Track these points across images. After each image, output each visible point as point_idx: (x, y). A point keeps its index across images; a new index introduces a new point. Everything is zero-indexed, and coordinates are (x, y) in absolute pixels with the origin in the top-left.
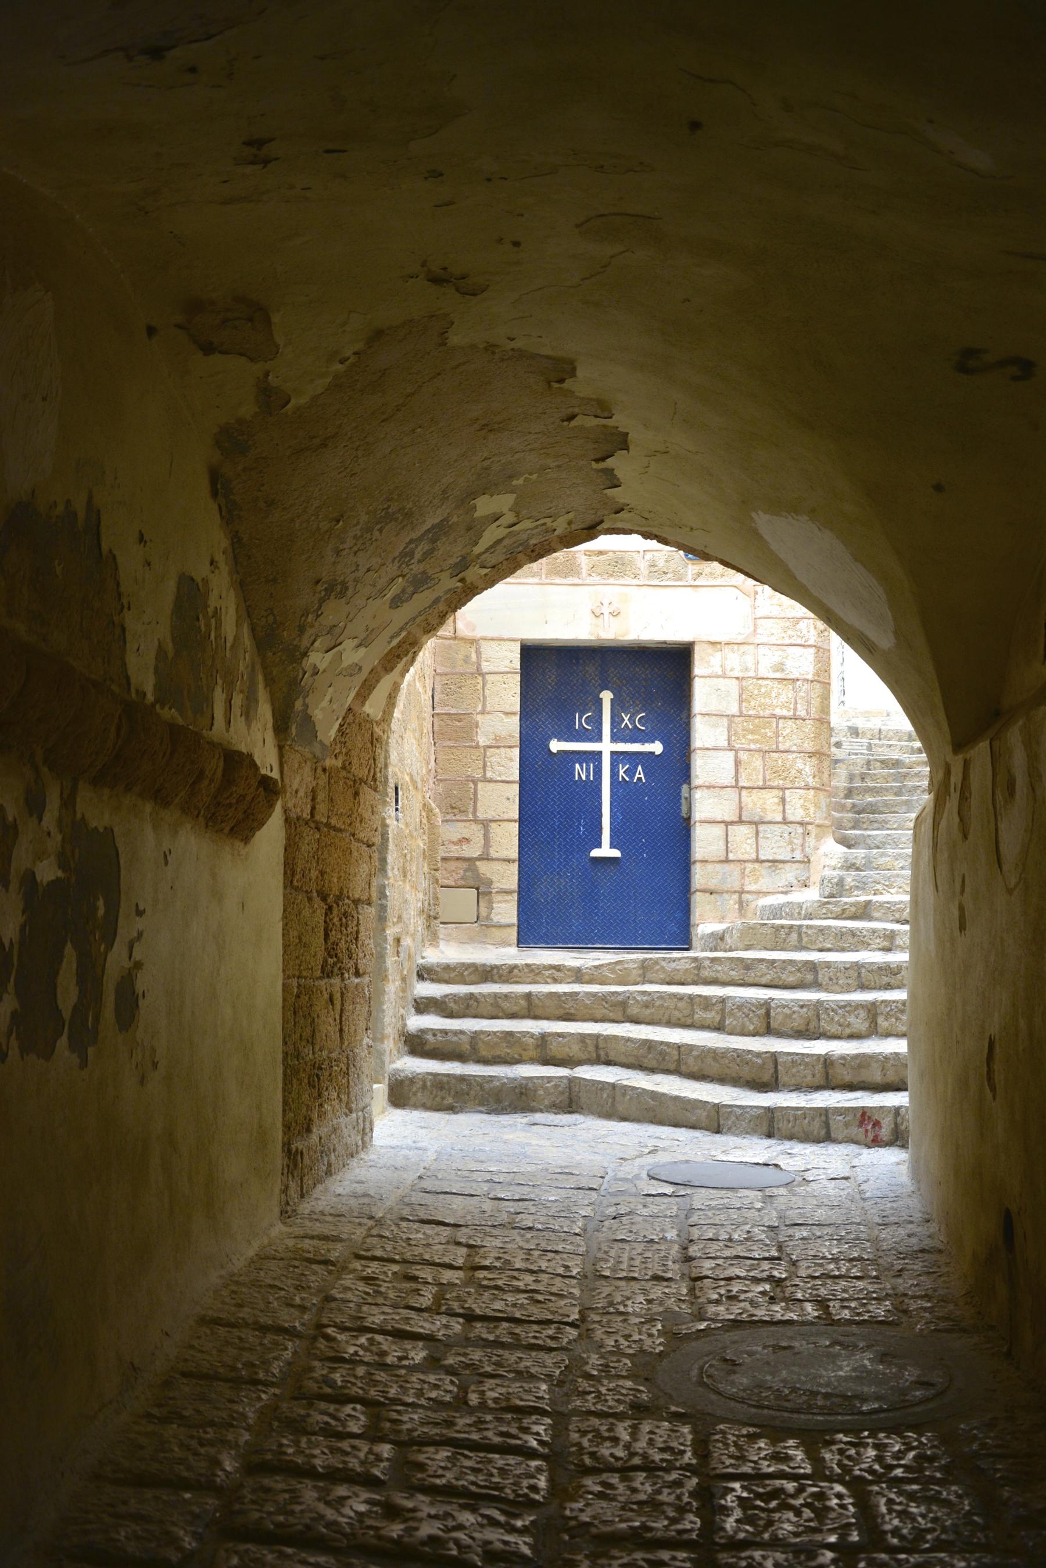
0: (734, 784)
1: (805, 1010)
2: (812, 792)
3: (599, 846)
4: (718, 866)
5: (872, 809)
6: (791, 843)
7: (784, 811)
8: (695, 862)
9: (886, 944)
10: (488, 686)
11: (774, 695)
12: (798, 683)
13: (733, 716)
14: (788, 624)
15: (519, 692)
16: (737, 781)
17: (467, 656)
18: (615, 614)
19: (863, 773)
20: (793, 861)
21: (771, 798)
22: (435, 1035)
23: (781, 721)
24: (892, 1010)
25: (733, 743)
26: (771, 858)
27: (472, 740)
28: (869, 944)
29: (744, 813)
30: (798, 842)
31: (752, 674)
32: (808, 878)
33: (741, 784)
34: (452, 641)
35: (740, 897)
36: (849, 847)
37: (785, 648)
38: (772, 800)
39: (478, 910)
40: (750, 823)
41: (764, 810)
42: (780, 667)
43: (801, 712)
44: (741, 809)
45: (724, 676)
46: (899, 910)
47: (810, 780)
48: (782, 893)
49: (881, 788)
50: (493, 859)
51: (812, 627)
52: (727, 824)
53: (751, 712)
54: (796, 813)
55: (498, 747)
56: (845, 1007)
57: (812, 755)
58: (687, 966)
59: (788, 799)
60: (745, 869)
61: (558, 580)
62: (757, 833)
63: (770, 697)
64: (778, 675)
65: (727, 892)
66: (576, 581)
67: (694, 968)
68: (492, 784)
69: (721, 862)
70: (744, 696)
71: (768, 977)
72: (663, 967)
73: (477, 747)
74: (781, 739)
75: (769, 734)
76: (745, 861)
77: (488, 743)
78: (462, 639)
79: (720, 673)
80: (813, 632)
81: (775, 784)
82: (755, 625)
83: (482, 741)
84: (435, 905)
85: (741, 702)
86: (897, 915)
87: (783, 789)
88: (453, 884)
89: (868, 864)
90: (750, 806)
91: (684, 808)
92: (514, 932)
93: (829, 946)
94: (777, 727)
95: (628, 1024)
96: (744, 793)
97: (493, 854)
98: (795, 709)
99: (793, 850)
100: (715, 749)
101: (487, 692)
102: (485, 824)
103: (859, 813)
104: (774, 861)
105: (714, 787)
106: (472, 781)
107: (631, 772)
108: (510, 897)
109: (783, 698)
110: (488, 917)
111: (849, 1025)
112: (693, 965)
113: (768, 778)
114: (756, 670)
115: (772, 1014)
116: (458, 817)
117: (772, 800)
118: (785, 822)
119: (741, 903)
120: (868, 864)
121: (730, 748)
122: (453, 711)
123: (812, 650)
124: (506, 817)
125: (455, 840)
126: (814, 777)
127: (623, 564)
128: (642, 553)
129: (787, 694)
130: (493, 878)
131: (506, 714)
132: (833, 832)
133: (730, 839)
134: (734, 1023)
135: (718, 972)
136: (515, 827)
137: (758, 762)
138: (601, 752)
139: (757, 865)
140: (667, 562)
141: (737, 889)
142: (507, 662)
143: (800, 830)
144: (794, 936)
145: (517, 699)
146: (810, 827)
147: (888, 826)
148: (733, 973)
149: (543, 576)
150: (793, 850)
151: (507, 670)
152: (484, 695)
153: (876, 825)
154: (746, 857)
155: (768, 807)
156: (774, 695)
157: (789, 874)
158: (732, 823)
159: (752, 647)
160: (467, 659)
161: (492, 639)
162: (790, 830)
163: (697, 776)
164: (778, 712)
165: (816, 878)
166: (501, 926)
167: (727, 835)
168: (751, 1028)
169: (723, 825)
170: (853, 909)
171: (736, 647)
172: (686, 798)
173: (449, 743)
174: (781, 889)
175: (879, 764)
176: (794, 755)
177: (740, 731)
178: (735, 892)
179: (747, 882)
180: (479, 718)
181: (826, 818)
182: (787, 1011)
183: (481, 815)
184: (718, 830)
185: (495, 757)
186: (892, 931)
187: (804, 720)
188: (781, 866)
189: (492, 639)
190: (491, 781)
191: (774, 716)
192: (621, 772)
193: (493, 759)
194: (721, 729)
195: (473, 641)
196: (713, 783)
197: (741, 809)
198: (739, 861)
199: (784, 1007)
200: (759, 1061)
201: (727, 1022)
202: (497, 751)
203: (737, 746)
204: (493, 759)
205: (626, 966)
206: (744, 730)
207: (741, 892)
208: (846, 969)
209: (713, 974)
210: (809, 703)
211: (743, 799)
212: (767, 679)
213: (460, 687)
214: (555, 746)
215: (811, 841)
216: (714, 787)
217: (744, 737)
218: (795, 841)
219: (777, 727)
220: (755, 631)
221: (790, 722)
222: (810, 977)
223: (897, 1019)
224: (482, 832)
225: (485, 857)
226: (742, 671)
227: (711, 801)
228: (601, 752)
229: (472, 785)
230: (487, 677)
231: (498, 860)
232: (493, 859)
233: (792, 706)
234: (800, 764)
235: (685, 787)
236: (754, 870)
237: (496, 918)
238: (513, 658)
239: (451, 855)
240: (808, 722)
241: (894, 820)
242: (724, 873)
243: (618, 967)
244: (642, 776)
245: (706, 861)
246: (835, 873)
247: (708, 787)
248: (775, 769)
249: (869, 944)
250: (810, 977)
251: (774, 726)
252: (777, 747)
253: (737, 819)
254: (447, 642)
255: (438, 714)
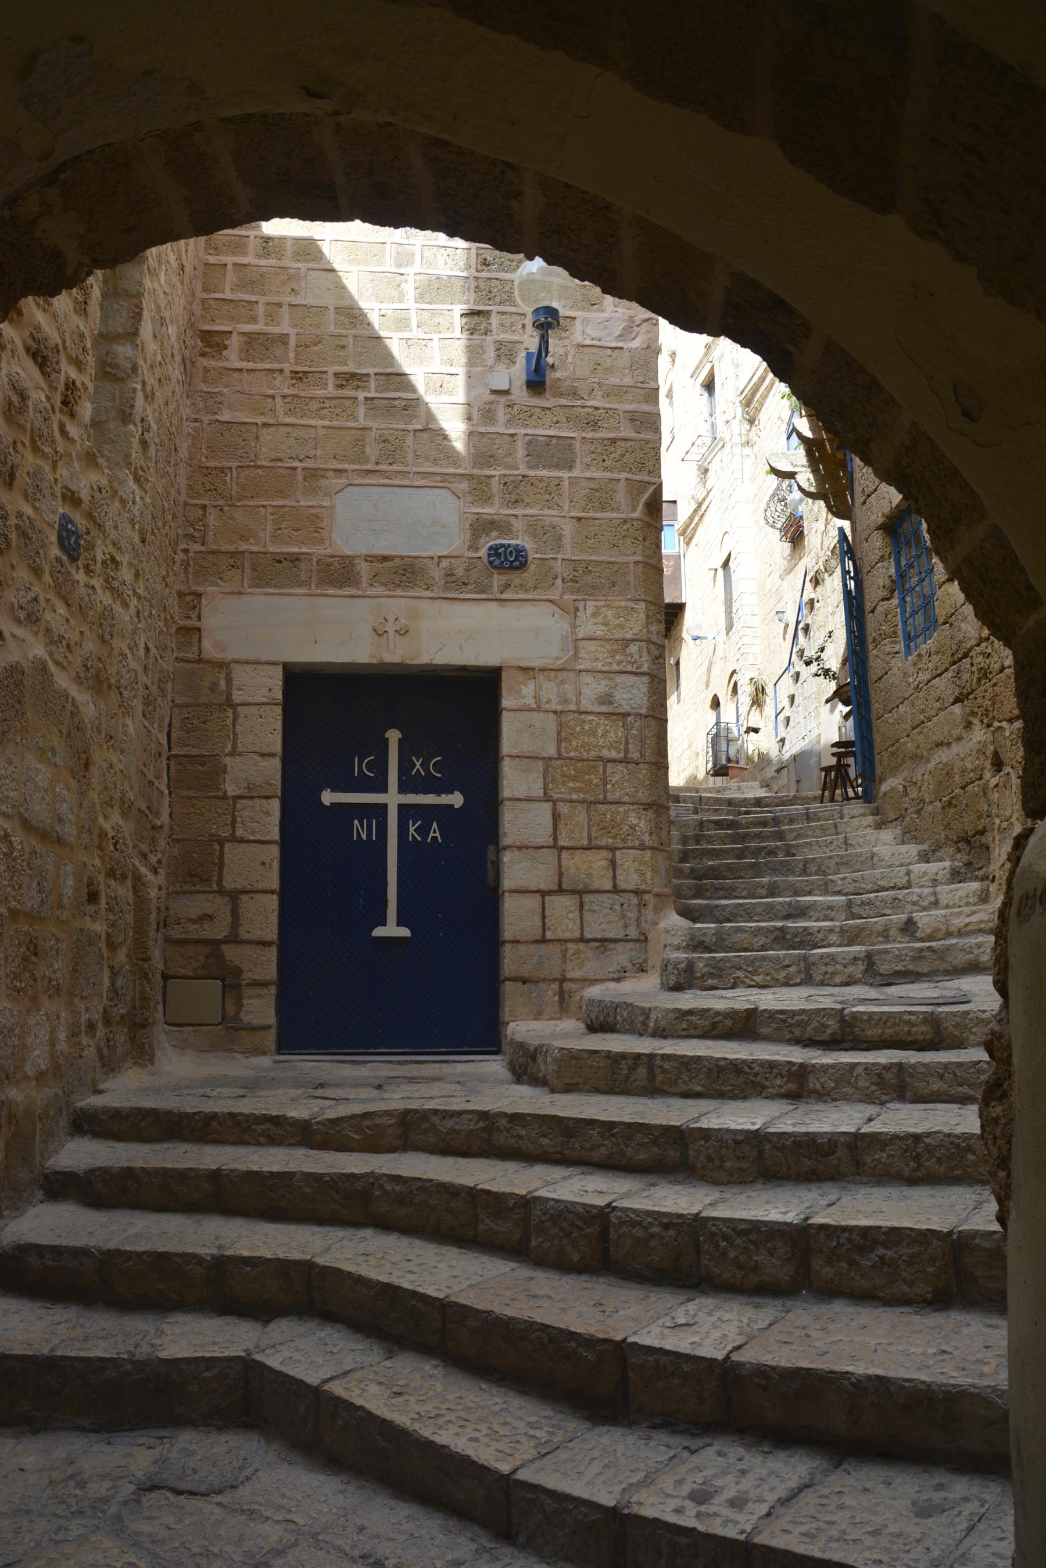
0: (552, 843)
1: (672, 1233)
2: (649, 853)
3: (384, 923)
4: (533, 948)
5: (715, 873)
6: (623, 917)
7: (614, 877)
8: (504, 942)
9: (792, 1086)
10: (240, 721)
11: (600, 733)
12: (630, 719)
13: (550, 759)
14: (615, 647)
15: (280, 728)
16: (555, 839)
17: (214, 684)
18: (403, 632)
19: (697, 835)
20: (626, 940)
21: (598, 861)
22: (41, 1256)
23: (609, 765)
24: (840, 1245)
25: (551, 793)
26: (599, 936)
27: (218, 789)
28: (764, 1088)
29: (565, 880)
30: (632, 915)
31: (572, 707)
32: (645, 961)
33: (561, 843)
34: (196, 665)
35: (561, 987)
36: (694, 920)
37: (613, 675)
38: (599, 863)
39: (223, 1008)
40: (573, 892)
41: (589, 875)
42: (606, 699)
43: (634, 755)
44: (561, 874)
45: (538, 709)
46: (799, 1024)
47: (646, 837)
48: (613, 980)
49: (721, 850)
50: (242, 942)
51: (645, 651)
52: (544, 894)
53: (572, 754)
54: (629, 879)
55: (252, 798)
56: (746, 1232)
57: (647, 807)
58: (472, 1127)
59: (619, 862)
60: (566, 950)
61: (331, 592)
62: (582, 905)
63: (595, 735)
64: (604, 709)
65: (544, 980)
66: (355, 592)
67: (482, 1129)
68: (243, 845)
69: (536, 942)
70: (563, 734)
71: (603, 1150)
72: (433, 1125)
73: (225, 797)
74: (609, 787)
75: (595, 781)
76: (566, 941)
77: (239, 793)
78: (209, 662)
79: (534, 706)
80: (646, 657)
81: (603, 843)
82: (576, 649)
83: (231, 790)
84: (142, 1008)
85: (559, 741)
86: (797, 1032)
87: (612, 849)
88: (191, 974)
89: (720, 943)
90: (573, 870)
91: (491, 875)
92: (272, 1036)
93: (699, 1088)
94: (605, 772)
95: (369, 1232)
96: (565, 854)
97: (244, 935)
98: (626, 751)
99: (626, 926)
100: (529, 800)
101: (239, 728)
102: (234, 896)
103: (700, 879)
104: (603, 940)
105: (527, 848)
106: (217, 841)
107: (423, 831)
108: (265, 991)
109: (612, 737)
110: (236, 1017)
111: (756, 1268)
112: (481, 1124)
113: (594, 835)
114: (578, 703)
115: (613, 1235)
116: (198, 888)
117: (599, 863)
118: (616, 890)
119: (561, 993)
120: (720, 943)
121: (547, 798)
122: (195, 752)
123: (646, 679)
124: (260, 886)
125: (194, 917)
126: (651, 834)
127: (413, 573)
128: (436, 559)
129: (615, 732)
130: (244, 967)
131: (263, 755)
132: (674, 902)
133: (547, 914)
134: (546, 1245)
135: (521, 1137)
136: (272, 902)
137: (581, 816)
138: (386, 805)
139: (581, 946)
140: (467, 570)
141: (557, 976)
142: (265, 691)
143: (635, 900)
144: (642, 1072)
145: (278, 738)
146: (646, 897)
147: (736, 894)
148: (545, 1141)
149: (313, 586)
150: (626, 926)
151: (264, 700)
152: (234, 733)
153: (722, 893)
154: (567, 935)
155: (594, 872)
156: (600, 733)
157: (622, 956)
158: (550, 892)
159: (572, 675)
160: (214, 687)
161: (247, 662)
162: (622, 900)
163: (505, 834)
164: (605, 753)
165: (655, 960)
166: (253, 1029)
167: (544, 908)
168: (576, 1257)
169: (538, 895)
170: (729, 1023)
171: (553, 674)
172: (493, 862)
173: (187, 793)
174: (612, 975)
175: (712, 825)
176: (626, 808)
177: (559, 778)
178: (554, 980)
179: (569, 968)
180: (228, 760)
181: (666, 886)
182: (637, 1231)
183: (228, 885)
184: (532, 903)
185: (247, 810)
186: (802, 1066)
187: (637, 764)
188: (611, 946)
189: (247, 662)
190: (242, 841)
191: (600, 758)
192: (412, 830)
193: (246, 813)
194: (535, 775)
195: (223, 665)
196: (526, 843)
197: (561, 874)
198: (559, 941)
199: (634, 1224)
200: (590, 1356)
201: (533, 1243)
202: (250, 802)
203: (556, 796)
204: (246, 813)
205: (378, 1121)
206: (563, 776)
207: (562, 980)
208: (737, 1143)
209: (513, 1142)
210: (643, 743)
211: (564, 862)
212: (591, 713)
213: (204, 722)
214: (328, 797)
215: (648, 914)
216: (527, 848)
217: (564, 784)
218: (629, 914)
219: (605, 772)
220: (576, 654)
221: (620, 767)
222: (673, 1154)
223: (852, 1264)
224: (229, 906)
225: (234, 939)
226: (560, 703)
227: (522, 865)
228: (386, 805)
229: (217, 847)
230: (239, 709)
231: (249, 942)
232: (242, 942)
233: (622, 747)
234: (633, 819)
235: (491, 848)
236: (578, 951)
237: (246, 1018)
238: (274, 684)
239: (189, 936)
240: (642, 766)
241: (743, 886)
242: (541, 957)
243: (366, 1123)
244: (438, 834)
245: (518, 942)
246: (682, 955)
247: (519, 848)
248: (603, 824)
249: (764, 1088)
250: (673, 1154)
251: (601, 771)
252: (605, 797)
253: (555, 888)
254: (190, 666)
255: (175, 756)
